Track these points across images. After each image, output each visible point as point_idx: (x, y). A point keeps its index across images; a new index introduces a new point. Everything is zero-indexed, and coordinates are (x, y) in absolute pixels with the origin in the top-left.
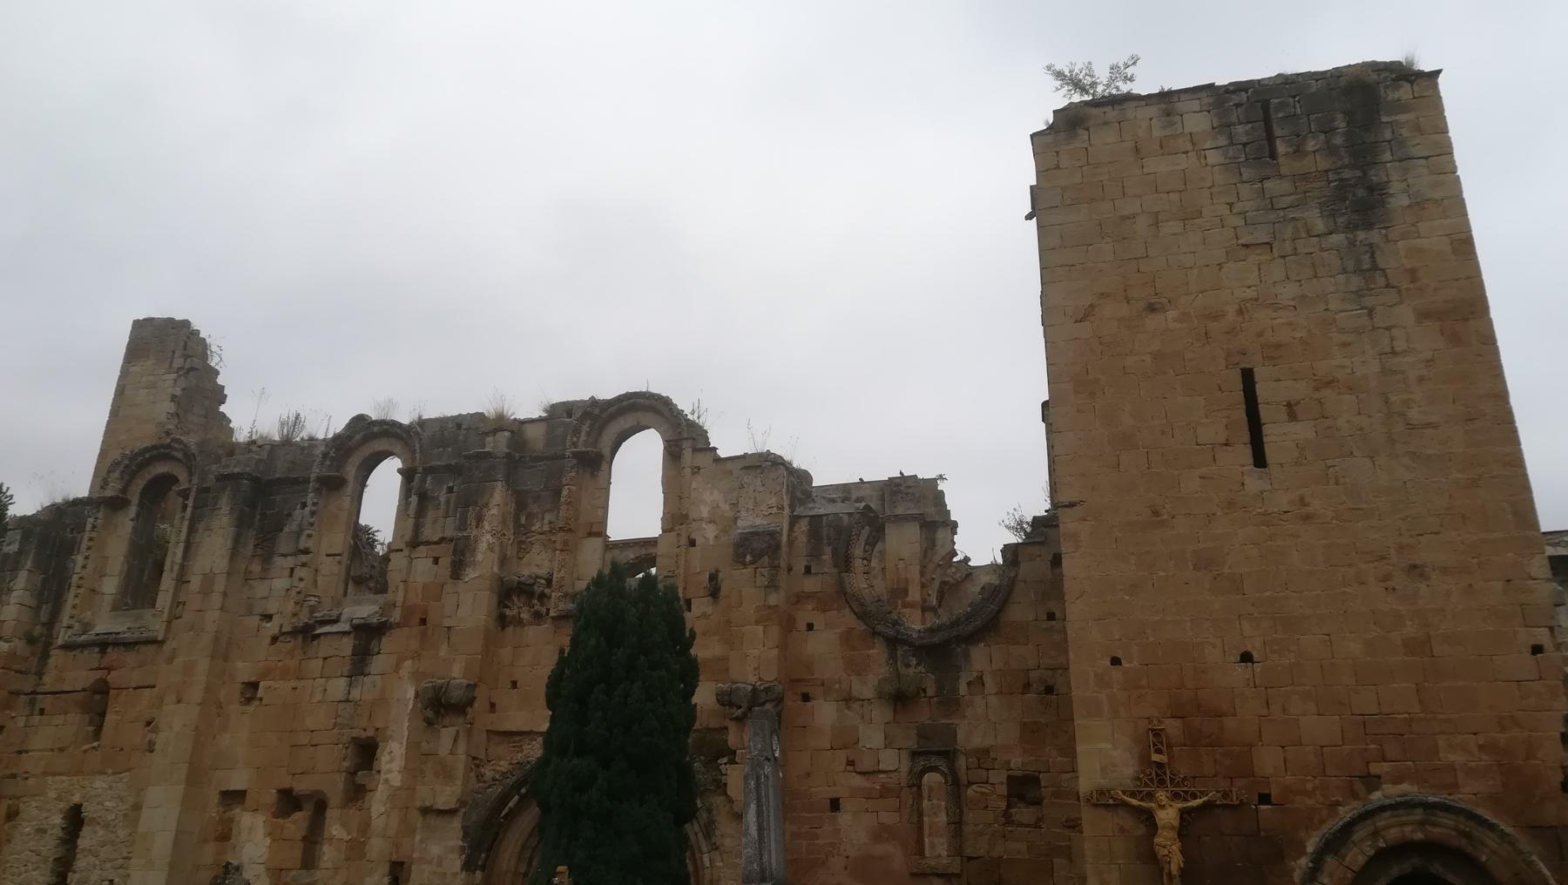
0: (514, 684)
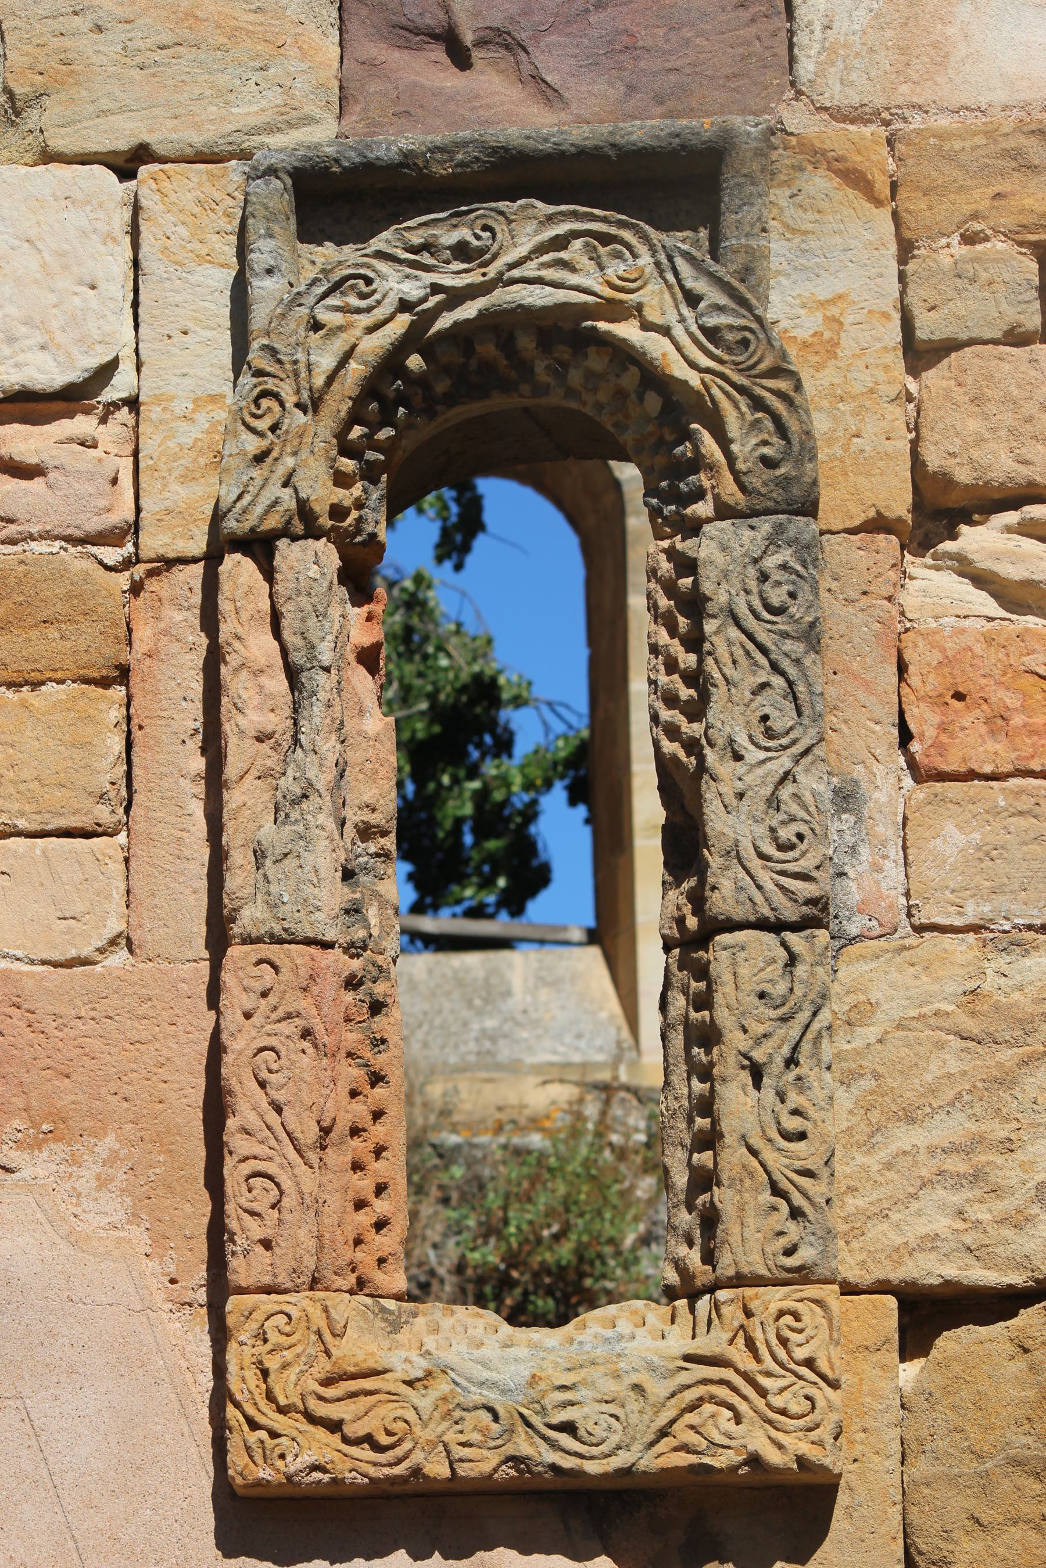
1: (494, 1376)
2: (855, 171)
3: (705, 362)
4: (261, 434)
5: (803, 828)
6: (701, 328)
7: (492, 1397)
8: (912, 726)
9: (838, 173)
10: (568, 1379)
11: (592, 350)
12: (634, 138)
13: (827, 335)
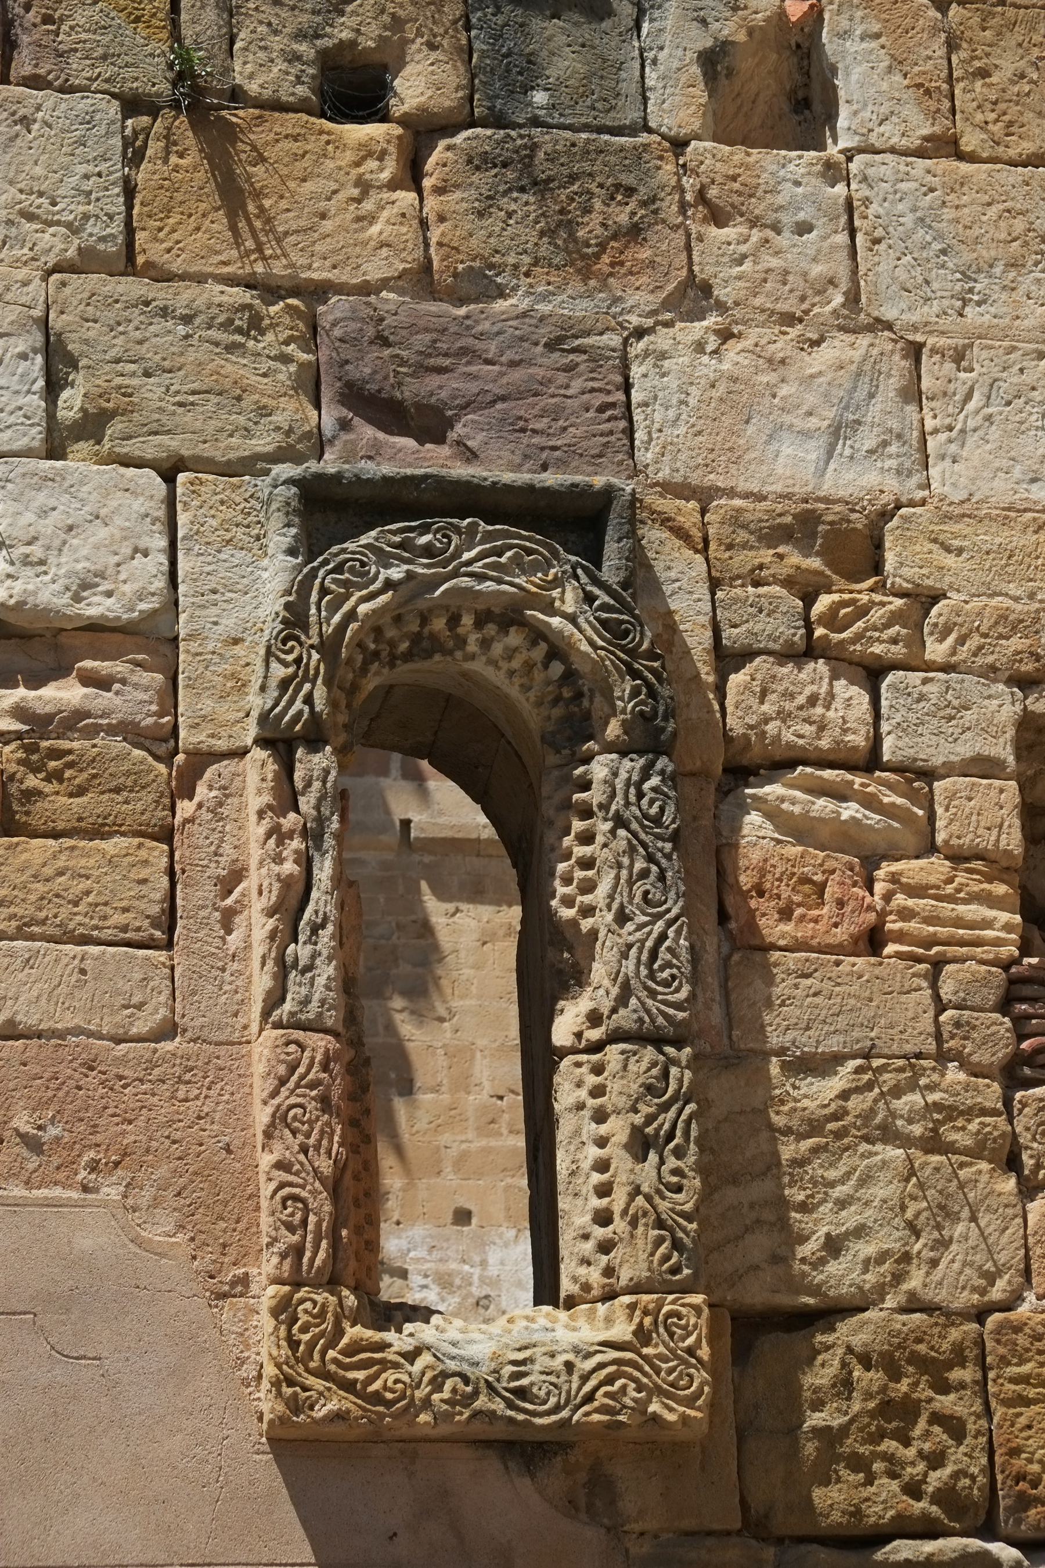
0: (463, 1217)
1: (462, 1352)
2: (680, 528)
3: (601, 643)
4: (286, 664)
5: (675, 971)
6: (596, 618)
7: (465, 1368)
8: (731, 911)
9: (671, 529)
10: (520, 1356)
11: (513, 630)
12: (547, 484)
13: (665, 637)
